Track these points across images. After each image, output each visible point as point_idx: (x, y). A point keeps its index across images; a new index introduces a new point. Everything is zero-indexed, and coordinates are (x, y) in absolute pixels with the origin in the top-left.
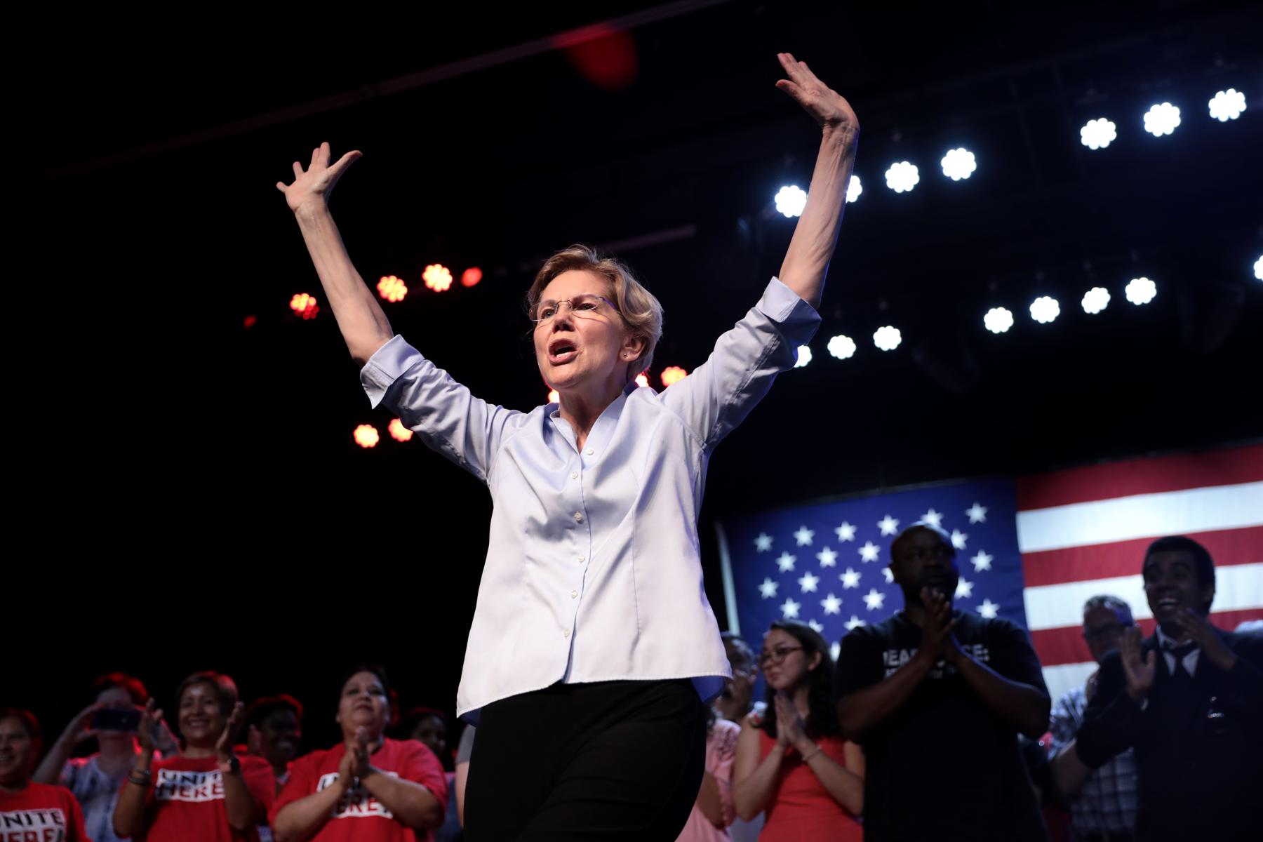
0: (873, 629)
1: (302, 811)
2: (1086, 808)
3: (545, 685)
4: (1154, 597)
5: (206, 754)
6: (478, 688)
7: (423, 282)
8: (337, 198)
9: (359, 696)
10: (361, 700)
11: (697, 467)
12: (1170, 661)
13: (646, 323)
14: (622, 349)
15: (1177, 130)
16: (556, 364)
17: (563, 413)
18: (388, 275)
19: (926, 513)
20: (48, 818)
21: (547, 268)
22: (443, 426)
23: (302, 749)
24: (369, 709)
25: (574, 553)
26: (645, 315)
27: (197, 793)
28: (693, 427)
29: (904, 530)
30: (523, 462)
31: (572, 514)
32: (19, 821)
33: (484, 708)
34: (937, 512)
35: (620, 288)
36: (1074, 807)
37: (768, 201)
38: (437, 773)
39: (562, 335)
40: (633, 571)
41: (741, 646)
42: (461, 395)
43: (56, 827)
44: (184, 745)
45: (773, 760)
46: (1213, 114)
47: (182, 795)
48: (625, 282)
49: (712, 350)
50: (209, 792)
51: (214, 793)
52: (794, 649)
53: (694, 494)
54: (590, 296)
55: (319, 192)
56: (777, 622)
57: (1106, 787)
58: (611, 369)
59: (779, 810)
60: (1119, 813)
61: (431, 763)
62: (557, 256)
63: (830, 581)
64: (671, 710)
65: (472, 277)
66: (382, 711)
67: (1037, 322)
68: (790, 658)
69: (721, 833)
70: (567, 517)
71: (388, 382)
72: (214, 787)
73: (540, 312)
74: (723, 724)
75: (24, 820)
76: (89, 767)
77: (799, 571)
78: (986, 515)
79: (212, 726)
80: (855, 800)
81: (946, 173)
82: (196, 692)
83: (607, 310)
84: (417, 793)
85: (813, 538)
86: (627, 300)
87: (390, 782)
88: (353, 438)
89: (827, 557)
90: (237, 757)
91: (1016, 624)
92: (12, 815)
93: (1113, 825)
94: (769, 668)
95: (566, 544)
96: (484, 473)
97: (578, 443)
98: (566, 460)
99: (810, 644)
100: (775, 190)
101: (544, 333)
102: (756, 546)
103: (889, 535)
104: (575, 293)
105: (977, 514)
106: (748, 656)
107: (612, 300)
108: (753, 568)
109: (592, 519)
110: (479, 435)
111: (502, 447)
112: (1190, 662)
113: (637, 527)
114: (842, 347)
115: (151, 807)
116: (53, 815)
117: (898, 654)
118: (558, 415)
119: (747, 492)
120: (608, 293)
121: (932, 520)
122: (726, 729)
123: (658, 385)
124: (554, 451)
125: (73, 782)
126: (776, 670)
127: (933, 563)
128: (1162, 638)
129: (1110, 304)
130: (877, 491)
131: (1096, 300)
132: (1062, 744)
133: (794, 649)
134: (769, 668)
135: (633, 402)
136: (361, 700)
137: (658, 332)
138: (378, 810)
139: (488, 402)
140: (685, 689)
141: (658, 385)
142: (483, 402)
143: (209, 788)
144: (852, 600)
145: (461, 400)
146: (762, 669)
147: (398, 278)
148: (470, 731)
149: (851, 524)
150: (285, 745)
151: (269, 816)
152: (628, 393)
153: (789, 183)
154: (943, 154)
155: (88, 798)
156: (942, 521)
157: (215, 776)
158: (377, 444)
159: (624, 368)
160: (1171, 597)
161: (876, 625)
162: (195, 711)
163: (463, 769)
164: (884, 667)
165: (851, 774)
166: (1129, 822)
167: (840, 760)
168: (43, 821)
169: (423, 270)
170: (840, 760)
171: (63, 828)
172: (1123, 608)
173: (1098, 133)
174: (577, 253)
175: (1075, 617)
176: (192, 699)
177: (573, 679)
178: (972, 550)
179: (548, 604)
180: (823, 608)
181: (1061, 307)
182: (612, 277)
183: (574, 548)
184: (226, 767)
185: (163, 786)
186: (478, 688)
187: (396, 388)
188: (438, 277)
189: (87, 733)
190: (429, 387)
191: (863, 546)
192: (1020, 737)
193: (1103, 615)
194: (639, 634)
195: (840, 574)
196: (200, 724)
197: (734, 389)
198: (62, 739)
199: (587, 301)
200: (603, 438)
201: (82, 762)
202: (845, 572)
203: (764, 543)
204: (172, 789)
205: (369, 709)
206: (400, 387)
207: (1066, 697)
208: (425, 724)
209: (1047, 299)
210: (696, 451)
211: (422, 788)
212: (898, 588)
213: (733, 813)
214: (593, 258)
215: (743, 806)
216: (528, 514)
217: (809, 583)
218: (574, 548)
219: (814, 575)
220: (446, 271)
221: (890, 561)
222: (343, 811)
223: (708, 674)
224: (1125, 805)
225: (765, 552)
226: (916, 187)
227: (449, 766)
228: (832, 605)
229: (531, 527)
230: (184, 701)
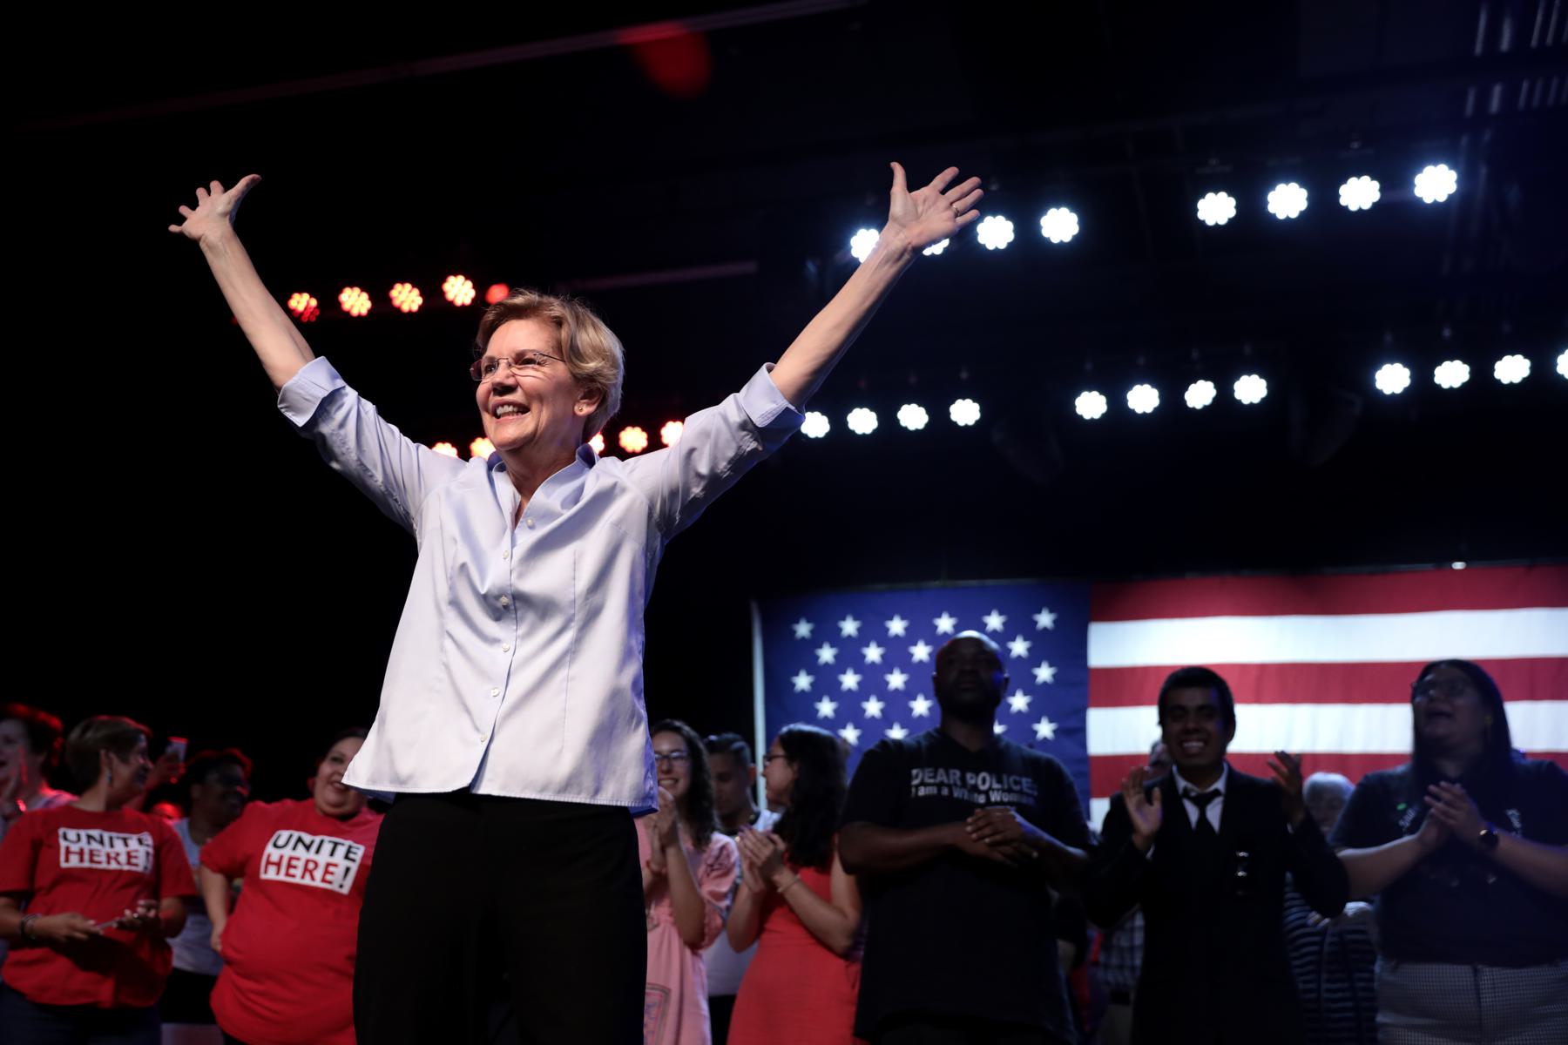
7: (443, 294)
8: (244, 222)
12: (1193, 813)
14: (576, 402)
15: (1010, 245)
20: (341, 851)
32: (102, 842)
39: (498, 398)
40: (111, 779)
43: (344, 864)
46: (1343, 202)
50: (318, 874)
55: (224, 215)
63: (873, 681)
77: (840, 666)
78: (1004, 624)
81: (1045, 233)
85: (859, 630)
92: (307, 838)
105: (1045, 619)
112: (1214, 813)
114: (863, 421)
117: (936, 773)
128: (1182, 784)
129: (1215, 399)
130: (937, 583)
131: (1200, 394)
144: (897, 705)
160: (1198, 740)
167: (825, 895)
168: (332, 854)
169: (444, 280)
170: (825, 895)
173: (1216, 209)
177: (484, 789)
178: (1034, 659)
203: (803, 629)
209: (1147, 387)
217: (850, 680)
220: (469, 284)
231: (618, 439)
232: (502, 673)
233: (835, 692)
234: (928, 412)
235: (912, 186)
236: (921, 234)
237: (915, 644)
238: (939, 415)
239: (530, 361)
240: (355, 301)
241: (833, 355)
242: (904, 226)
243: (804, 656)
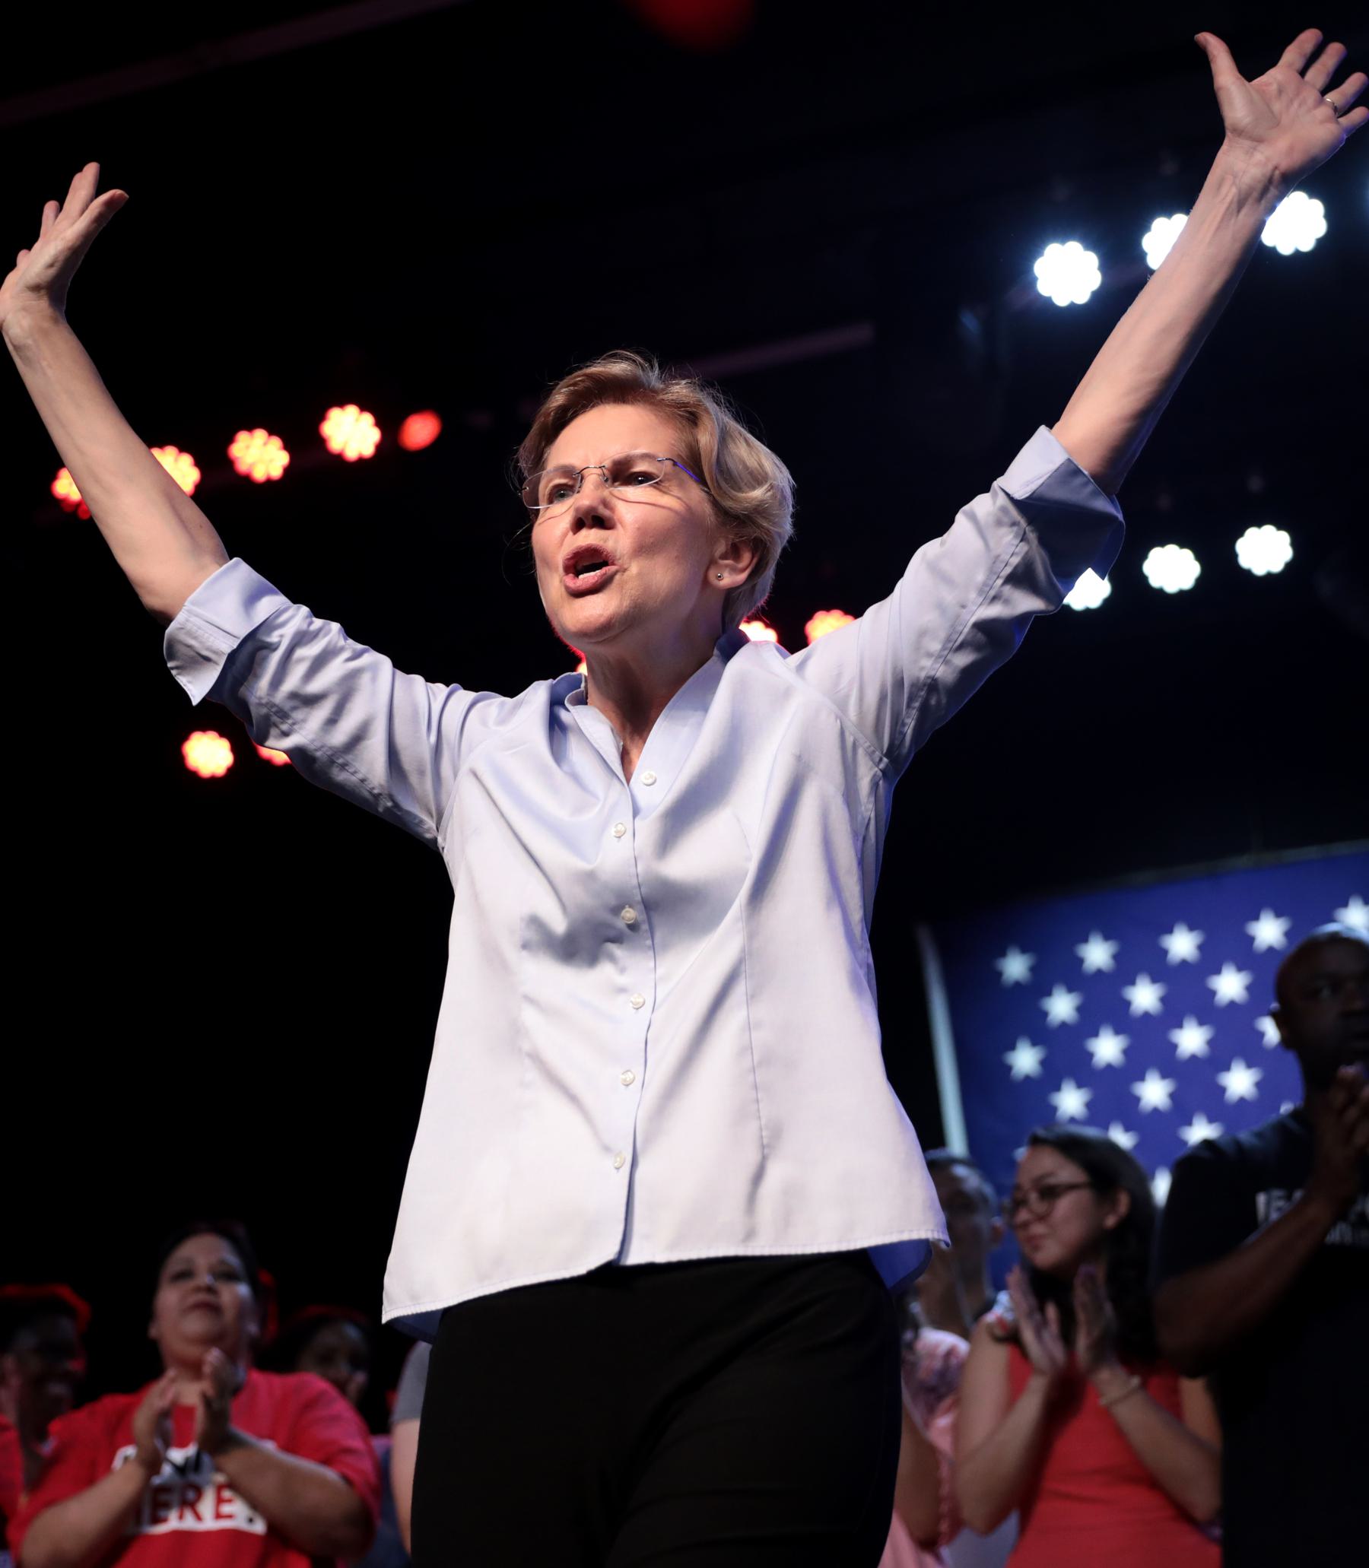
0: (1238, 1145)
3: (580, 1268)
7: (321, 442)
9: (191, 1284)
11: (867, 808)
13: (760, 510)
14: (712, 562)
16: (578, 594)
17: (593, 695)
18: (250, 428)
19: (1345, 904)
23: (85, 1394)
24: (213, 1309)
25: (622, 990)
26: (758, 493)
28: (861, 723)
30: (512, 793)
31: (617, 910)
33: (447, 1312)
35: (706, 438)
37: (1020, 273)
38: (356, 1443)
39: (590, 537)
40: (749, 1027)
41: (969, 1178)
48: (718, 427)
49: (901, 575)
52: (1072, 1187)
53: (861, 862)
54: (646, 457)
56: (1041, 1132)
59: (1045, 1509)
61: (342, 1422)
62: (578, 376)
63: (1149, 1044)
65: (420, 430)
68: (1065, 1205)
69: (929, 1560)
70: (609, 917)
73: (544, 489)
74: (938, 1340)
77: (1088, 1023)
80: (1204, 1498)
83: (681, 485)
84: (322, 1483)
87: (268, 1462)
88: (180, 758)
95: (605, 971)
96: (430, 823)
97: (625, 757)
98: (601, 793)
99: (1105, 1171)
100: (1034, 250)
101: (554, 532)
103: (1271, 950)
104: (615, 450)
106: (984, 1199)
107: (691, 463)
109: (657, 919)
110: (416, 748)
111: (464, 768)
113: (751, 935)
114: (1172, 569)
118: (582, 700)
119: (974, 861)
120: (682, 449)
122: (942, 1349)
123: (793, 640)
124: (575, 777)
126: (1038, 1229)
130: (1244, 861)
134: (1025, 1225)
137: (785, 527)
138: (238, 1516)
140: (857, 1266)
141: (793, 640)
142: (418, 679)
144: (1196, 1084)
147: (271, 432)
149: (1192, 928)
150: (57, 1389)
151: (11, 1532)
152: (728, 654)
153: (1063, 236)
158: (230, 770)
159: (716, 604)
163: (407, 1436)
164: (1249, 1219)
165: (1196, 1442)
167: (1173, 1408)
170: (1173, 1408)
174: (618, 368)
177: (636, 1257)
179: (573, 1098)
182: (691, 417)
183: (621, 980)
188: (351, 432)
197: (935, 646)
199: (640, 467)
200: (674, 748)
202: (1180, 1026)
203: (1015, 967)
205: (213, 1309)
208: (327, 1338)
210: (866, 773)
211: (330, 1474)
213: (957, 1524)
215: (973, 1510)
216: (526, 910)
217: (1107, 1048)
218: (621, 980)
219: (1118, 1032)
220: (368, 419)
221: (1275, 1005)
222: (164, 1520)
223: (905, 1237)
225: (1017, 984)
226: (1321, 242)
228: (1154, 1092)
229: (532, 935)
231: (234, 749)
232: (646, 1040)
233: (1083, 1071)
234: (1199, 557)
235: (1251, 66)
237: (1218, 971)
238: (1218, 559)
239: (645, 478)
240: (260, 455)
242: (1260, 140)
243: (1021, 1013)
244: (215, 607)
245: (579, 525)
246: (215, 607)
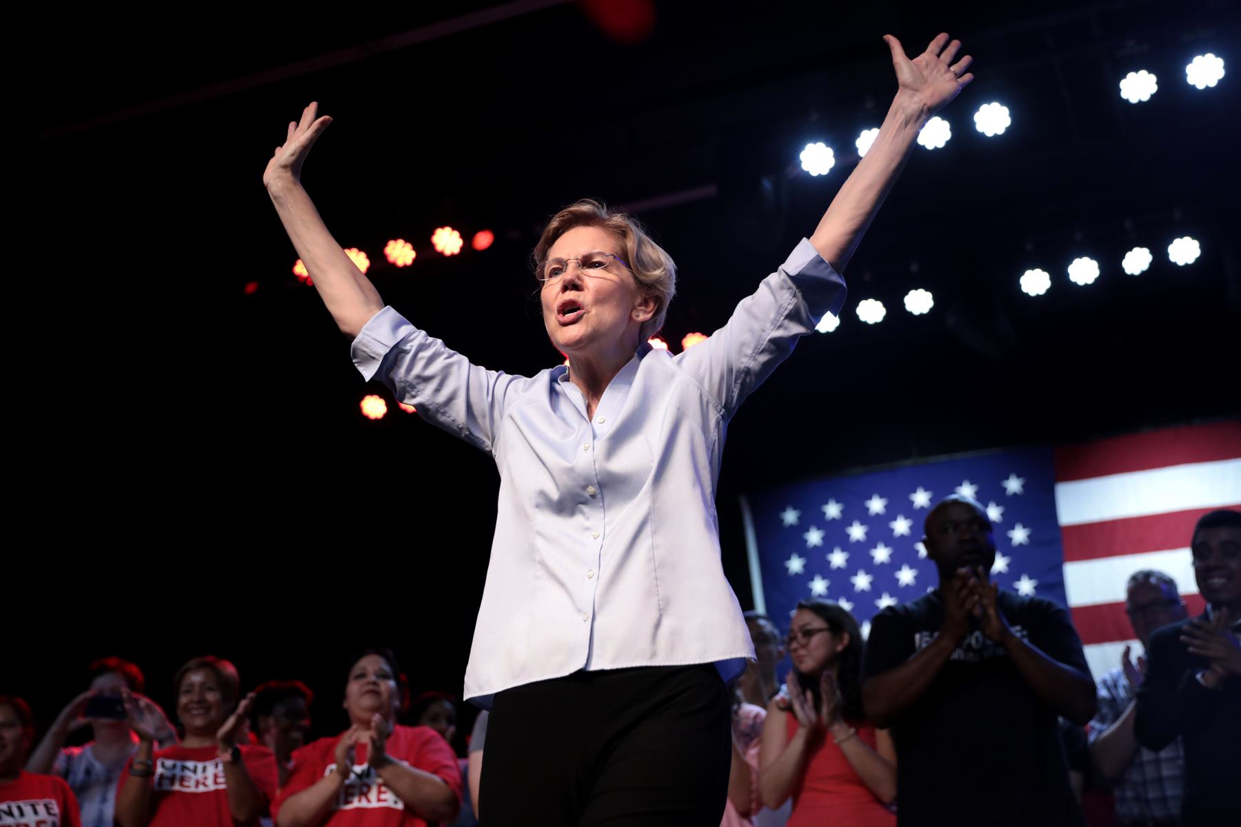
0: (906, 609)
1: (309, 799)
2: (1129, 794)
4: (1202, 575)
5: (207, 743)
6: (492, 669)
7: (432, 246)
9: (365, 680)
10: (369, 683)
11: (714, 435)
13: (659, 281)
14: (634, 308)
15: (1220, 82)
17: (572, 377)
18: (395, 239)
21: (554, 224)
22: (442, 397)
23: (310, 737)
24: (376, 693)
25: (587, 529)
26: (658, 272)
27: (197, 783)
29: (937, 503)
30: (530, 428)
31: (585, 487)
32: (10, 814)
33: (497, 694)
34: (972, 483)
35: (631, 244)
36: (1117, 793)
37: (793, 159)
38: (450, 762)
39: (571, 295)
40: (653, 548)
42: (459, 363)
43: (49, 819)
44: (182, 735)
45: (798, 744)
47: (182, 785)
48: (636, 234)
49: (731, 314)
50: (210, 782)
51: (216, 783)
52: (820, 630)
53: (711, 463)
54: (599, 253)
56: (803, 602)
57: (1150, 772)
58: (622, 329)
59: (806, 797)
60: (1164, 799)
61: (443, 751)
62: (564, 212)
63: (860, 557)
64: (705, 687)
65: (483, 240)
66: (391, 695)
67: (1075, 284)
68: (816, 640)
69: (746, 823)
71: (383, 351)
72: (216, 776)
73: (547, 270)
74: (750, 709)
75: (16, 812)
76: (84, 756)
78: (1024, 486)
79: (213, 713)
80: (887, 790)
82: (196, 678)
83: (618, 268)
84: (433, 783)
86: (639, 258)
87: (405, 773)
88: (360, 409)
89: (857, 532)
90: (238, 746)
91: (1055, 601)
93: (1158, 812)
94: (796, 650)
95: (578, 519)
96: (488, 443)
97: (589, 409)
99: (837, 622)
100: (800, 148)
101: (552, 293)
102: (782, 521)
104: (584, 250)
105: (1014, 485)
106: (774, 636)
108: (780, 541)
109: (605, 492)
113: (654, 501)
114: (871, 311)
115: (154, 799)
116: (46, 806)
118: (567, 379)
119: (768, 461)
120: (618, 249)
121: (966, 492)
122: (752, 714)
123: (676, 348)
124: (563, 419)
125: (67, 773)
127: (967, 536)
129: (1152, 264)
130: (908, 462)
131: (1137, 261)
132: (1104, 727)
133: (820, 630)
134: (796, 650)
135: (649, 373)
136: (369, 683)
137: (672, 290)
138: (390, 800)
139: (488, 368)
140: (709, 671)
141: (676, 348)
142: (482, 368)
143: (207, 777)
144: (884, 577)
145: (459, 368)
146: (789, 651)
147: (406, 241)
148: (484, 715)
149: (881, 497)
151: (272, 809)
152: (642, 356)
153: (815, 140)
154: (976, 108)
155: (83, 789)
156: (977, 493)
157: (217, 766)
158: (385, 415)
159: (636, 330)
160: (1220, 577)
161: (908, 604)
162: (195, 698)
163: (476, 759)
166: (1175, 809)
167: (872, 744)
168: (36, 812)
169: (433, 233)
170: (872, 744)
171: (57, 820)
172: (1170, 584)
173: (1138, 87)
174: (585, 208)
175: (1117, 592)
176: (192, 685)
178: (1009, 522)
179: (562, 584)
180: (853, 585)
181: (1100, 268)
182: (623, 233)
183: (587, 524)
184: (227, 756)
185: (162, 776)
186: (492, 669)
187: (392, 357)
188: (447, 241)
189: (81, 721)
190: (426, 354)
191: (895, 519)
192: (1061, 719)
193: (1149, 592)
194: (661, 616)
195: (870, 548)
196: (201, 711)
198: (54, 728)
199: (597, 259)
200: (615, 404)
201: (76, 751)
202: (875, 547)
203: (790, 517)
204: (172, 780)
206: (395, 355)
207: (1107, 677)
208: (435, 708)
209: (1086, 260)
210: (713, 417)
211: (437, 778)
212: (933, 567)
213: (760, 805)
214: (603, 213)
216: (538, 487)
218: (587, 524)
219: (843, 550)
220: (456, 234)
222: (351, 802)
224: (1170, 791)
225: (791, 526)
226: (1008, 129)
227: (461, 750)
228: (862, 581)
230: (184, 688)
232: (596, 553)
235: (912, 53)
236: (933, 95)
239: (599, 264)
241: (869, 214)
242: (916, 90)
243: (794, 541)
244: (376, 329)
245: (565, 289)
246: (376, 329)
